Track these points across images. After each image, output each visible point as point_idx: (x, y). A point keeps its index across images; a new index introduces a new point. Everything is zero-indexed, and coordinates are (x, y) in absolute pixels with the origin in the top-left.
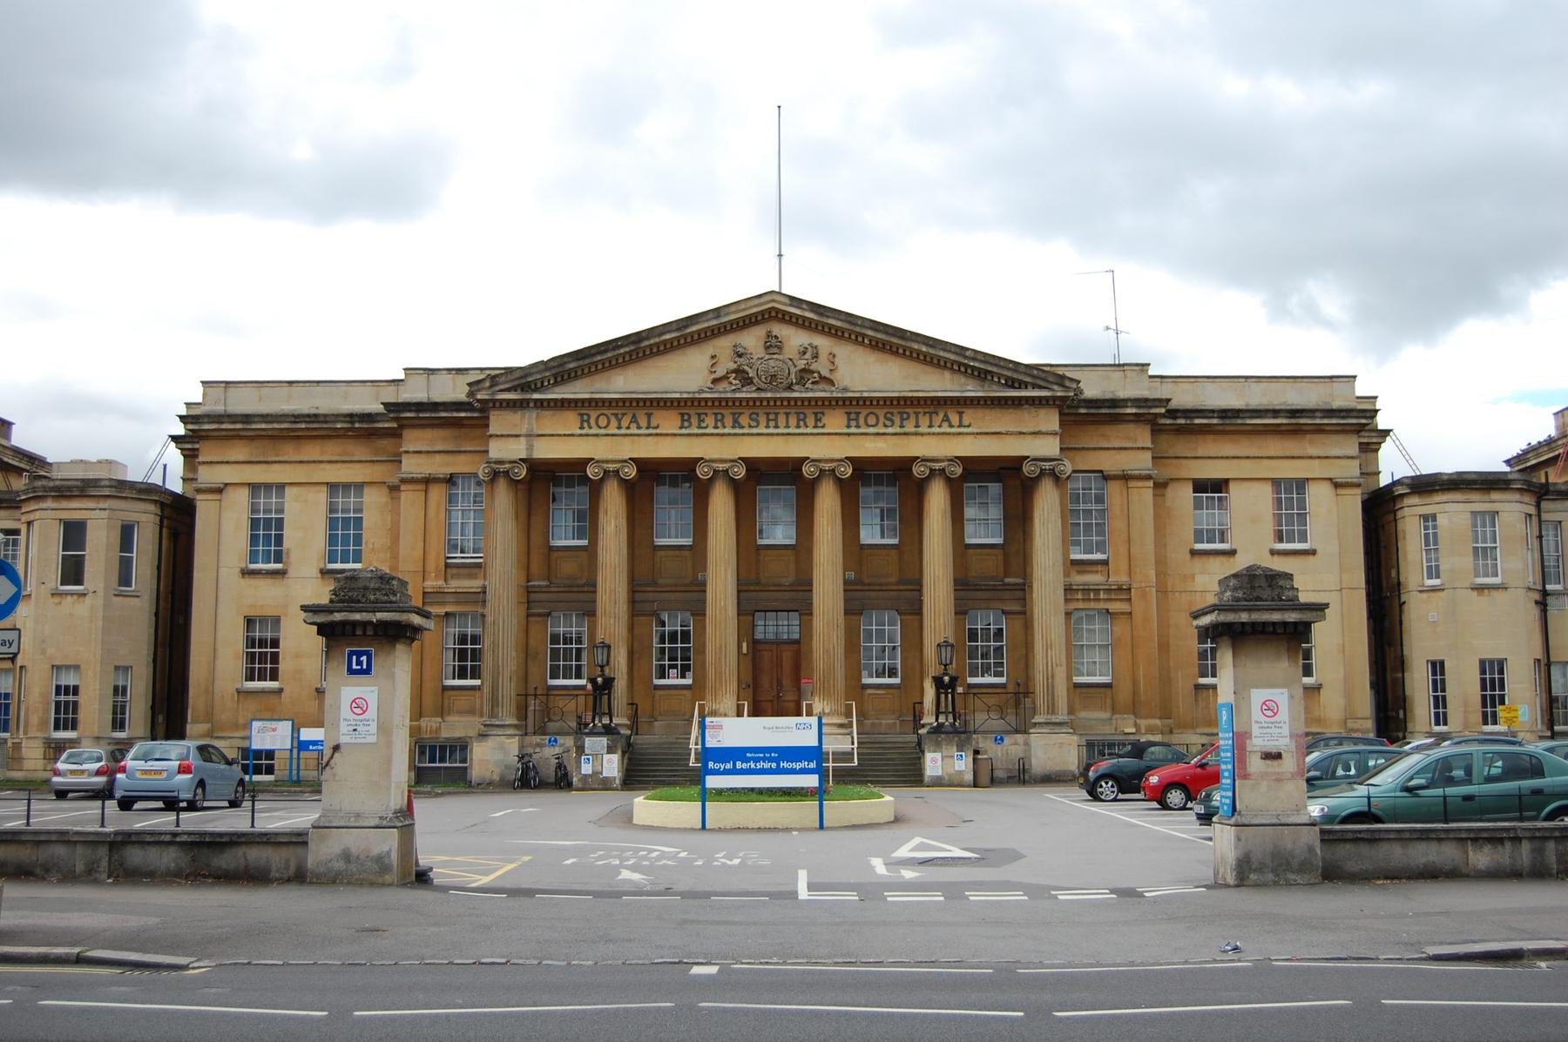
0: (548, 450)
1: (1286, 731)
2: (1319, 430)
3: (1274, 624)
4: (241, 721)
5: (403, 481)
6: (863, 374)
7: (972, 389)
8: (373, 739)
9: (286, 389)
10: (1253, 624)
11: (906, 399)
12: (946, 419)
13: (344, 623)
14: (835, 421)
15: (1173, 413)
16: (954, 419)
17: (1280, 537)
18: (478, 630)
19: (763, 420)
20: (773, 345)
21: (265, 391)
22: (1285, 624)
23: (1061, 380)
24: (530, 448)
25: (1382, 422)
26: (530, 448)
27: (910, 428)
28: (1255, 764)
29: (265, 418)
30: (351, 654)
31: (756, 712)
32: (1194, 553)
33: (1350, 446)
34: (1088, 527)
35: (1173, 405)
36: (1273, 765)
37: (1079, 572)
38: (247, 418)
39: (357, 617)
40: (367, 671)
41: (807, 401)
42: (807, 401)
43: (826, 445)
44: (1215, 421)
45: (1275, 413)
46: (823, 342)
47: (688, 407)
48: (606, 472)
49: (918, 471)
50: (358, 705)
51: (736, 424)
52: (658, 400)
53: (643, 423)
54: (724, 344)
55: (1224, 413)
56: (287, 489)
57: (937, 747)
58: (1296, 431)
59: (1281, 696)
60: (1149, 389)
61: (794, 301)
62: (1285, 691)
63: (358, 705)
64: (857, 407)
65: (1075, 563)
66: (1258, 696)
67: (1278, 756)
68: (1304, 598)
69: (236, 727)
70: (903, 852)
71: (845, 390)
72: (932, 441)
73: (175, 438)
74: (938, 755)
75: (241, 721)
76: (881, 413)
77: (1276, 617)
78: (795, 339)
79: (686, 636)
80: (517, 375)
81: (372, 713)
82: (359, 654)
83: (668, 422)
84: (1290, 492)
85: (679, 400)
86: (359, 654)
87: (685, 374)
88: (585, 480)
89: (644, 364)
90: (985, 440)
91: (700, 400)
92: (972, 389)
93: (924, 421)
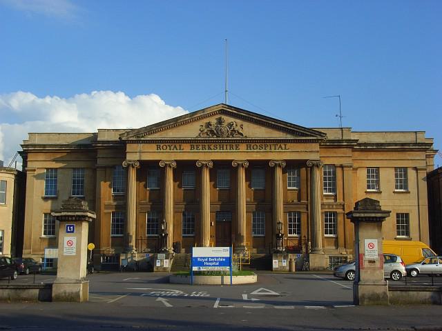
0: (146, 157)
1: (377, 253)
2: (412, 150)
3: (362, 217)
4: (42, 248)
5: (98, 167)
6: (253, 131)
7: (289, 137)
8: (74, 254)
9: (58, 135)
10: (365, 217)
11: (267, 140)
12: (280, 146)
13: (65, 216)
14: (243, 147)
15: (360, 145)
16: (283, 147)
17: (369, 187)
18: (122, 218)
19: (218, 147)
20: (220, 121)
21: (51, 136)
22: (376, 217)
23: (320, 134)
24: (140, 156)
25: (434, 147)
26: (140, 156)
27: (268, 150)
28: (366, 264)
29: (51, 146)
30: (67, 226)
31: (217, 245)
32: (394, 192)
33: (422, 155)
34: (51, 177)
35: (360, 142)
36: (372, 265)
37: (327, 199)
38: (44, 146)
39: (69, 214)
40: (73, 232)
41: (237, 141)
42: (237, 141)
43: (240, 155)
44: (374, 147)
45: (396, 144)
46: (239, 122)
47: (193, 142)
48: (166, 164)
49: (234, 164)
50: (70, 243)
51: (210, 148)
52: (183, 140)
53: (178, 148)
54: (206, 120)
55: (377, 144)
56: (58, 171)
57: (277, 258)
58: (403, 150)
59: (375, 242)
60: (49, 139)
61: (230, 107)
62: (376, 240)
63: (70, 243)
64: (250, 142)
65: (325, 196)
66: (367, 241)
67: (374, 262)
68: (383, 209)
69: (40, 251)
70: (255, 293)
71: (246, 137)
72: (276, 154)
73: (19, 152)
74: (277, 261)
75: (42, 248)
76: (178, 146)
77: (373, 215)
78: (228, 120)
79: (193, 219)
80: (136, 131)
81: (74, 245)
82: (70, 226)
83: (187, 147)
84: (374, 173)
85: (190, 140)
86: (70, 226)
87: (192, 131)
88: (307, 167)
89: (179, 128)
90: (294, 154)
91: (197, 140)
92: (289, 137)
93: (273, 147)
